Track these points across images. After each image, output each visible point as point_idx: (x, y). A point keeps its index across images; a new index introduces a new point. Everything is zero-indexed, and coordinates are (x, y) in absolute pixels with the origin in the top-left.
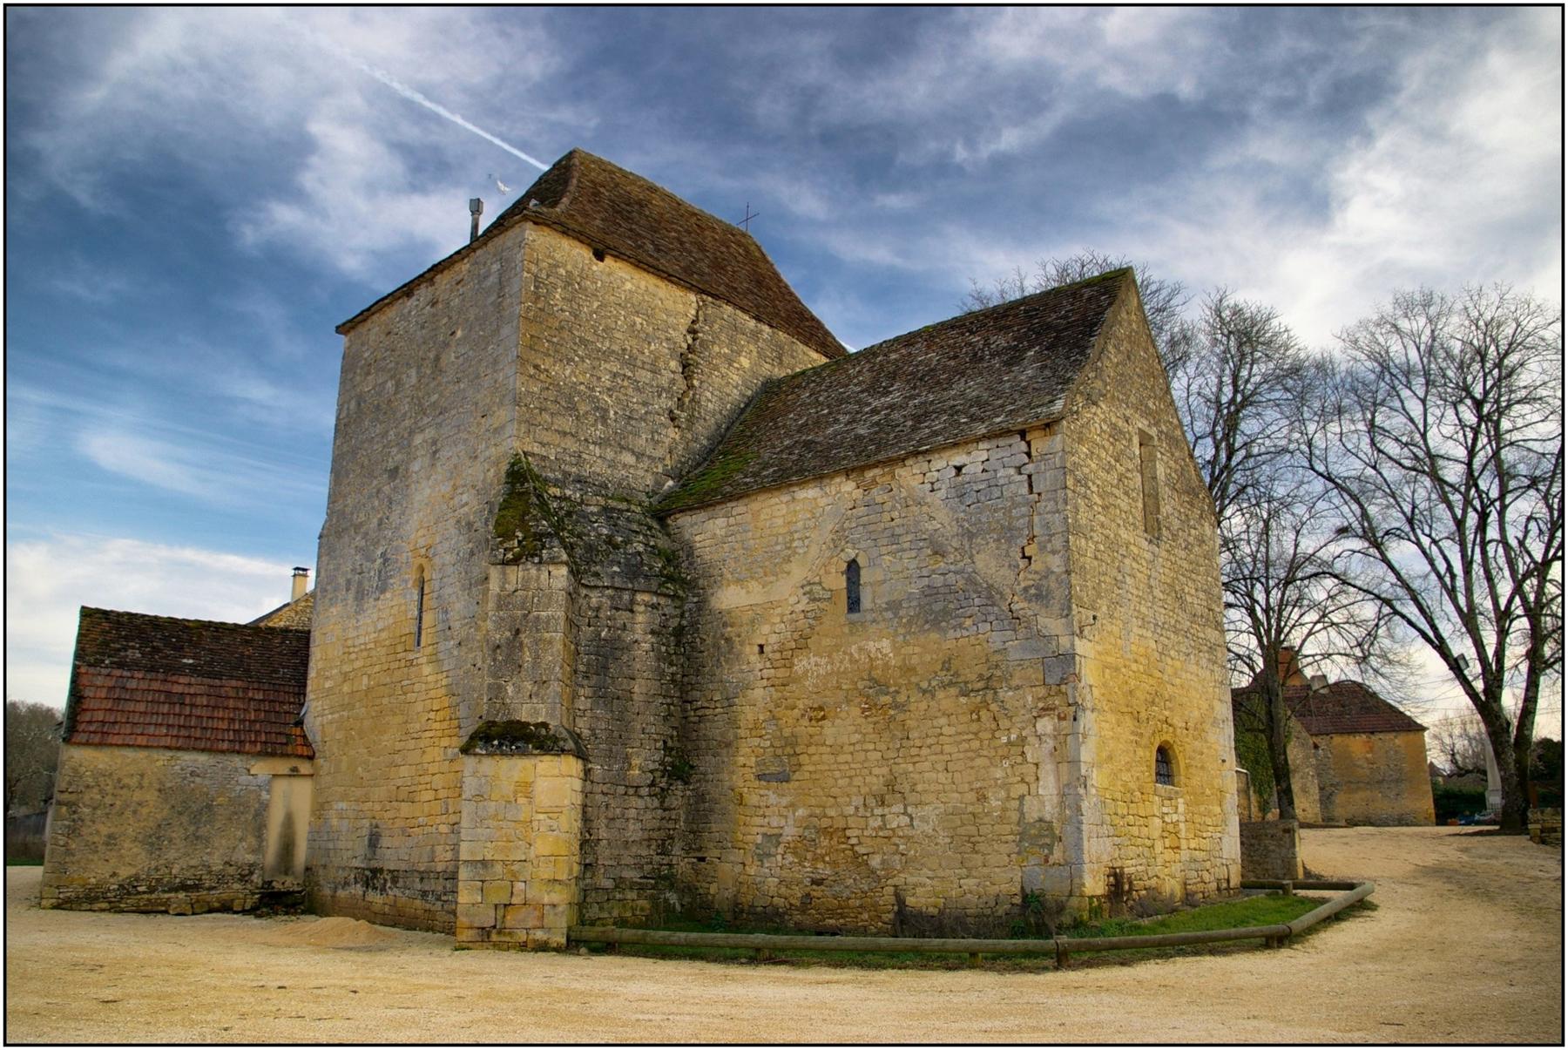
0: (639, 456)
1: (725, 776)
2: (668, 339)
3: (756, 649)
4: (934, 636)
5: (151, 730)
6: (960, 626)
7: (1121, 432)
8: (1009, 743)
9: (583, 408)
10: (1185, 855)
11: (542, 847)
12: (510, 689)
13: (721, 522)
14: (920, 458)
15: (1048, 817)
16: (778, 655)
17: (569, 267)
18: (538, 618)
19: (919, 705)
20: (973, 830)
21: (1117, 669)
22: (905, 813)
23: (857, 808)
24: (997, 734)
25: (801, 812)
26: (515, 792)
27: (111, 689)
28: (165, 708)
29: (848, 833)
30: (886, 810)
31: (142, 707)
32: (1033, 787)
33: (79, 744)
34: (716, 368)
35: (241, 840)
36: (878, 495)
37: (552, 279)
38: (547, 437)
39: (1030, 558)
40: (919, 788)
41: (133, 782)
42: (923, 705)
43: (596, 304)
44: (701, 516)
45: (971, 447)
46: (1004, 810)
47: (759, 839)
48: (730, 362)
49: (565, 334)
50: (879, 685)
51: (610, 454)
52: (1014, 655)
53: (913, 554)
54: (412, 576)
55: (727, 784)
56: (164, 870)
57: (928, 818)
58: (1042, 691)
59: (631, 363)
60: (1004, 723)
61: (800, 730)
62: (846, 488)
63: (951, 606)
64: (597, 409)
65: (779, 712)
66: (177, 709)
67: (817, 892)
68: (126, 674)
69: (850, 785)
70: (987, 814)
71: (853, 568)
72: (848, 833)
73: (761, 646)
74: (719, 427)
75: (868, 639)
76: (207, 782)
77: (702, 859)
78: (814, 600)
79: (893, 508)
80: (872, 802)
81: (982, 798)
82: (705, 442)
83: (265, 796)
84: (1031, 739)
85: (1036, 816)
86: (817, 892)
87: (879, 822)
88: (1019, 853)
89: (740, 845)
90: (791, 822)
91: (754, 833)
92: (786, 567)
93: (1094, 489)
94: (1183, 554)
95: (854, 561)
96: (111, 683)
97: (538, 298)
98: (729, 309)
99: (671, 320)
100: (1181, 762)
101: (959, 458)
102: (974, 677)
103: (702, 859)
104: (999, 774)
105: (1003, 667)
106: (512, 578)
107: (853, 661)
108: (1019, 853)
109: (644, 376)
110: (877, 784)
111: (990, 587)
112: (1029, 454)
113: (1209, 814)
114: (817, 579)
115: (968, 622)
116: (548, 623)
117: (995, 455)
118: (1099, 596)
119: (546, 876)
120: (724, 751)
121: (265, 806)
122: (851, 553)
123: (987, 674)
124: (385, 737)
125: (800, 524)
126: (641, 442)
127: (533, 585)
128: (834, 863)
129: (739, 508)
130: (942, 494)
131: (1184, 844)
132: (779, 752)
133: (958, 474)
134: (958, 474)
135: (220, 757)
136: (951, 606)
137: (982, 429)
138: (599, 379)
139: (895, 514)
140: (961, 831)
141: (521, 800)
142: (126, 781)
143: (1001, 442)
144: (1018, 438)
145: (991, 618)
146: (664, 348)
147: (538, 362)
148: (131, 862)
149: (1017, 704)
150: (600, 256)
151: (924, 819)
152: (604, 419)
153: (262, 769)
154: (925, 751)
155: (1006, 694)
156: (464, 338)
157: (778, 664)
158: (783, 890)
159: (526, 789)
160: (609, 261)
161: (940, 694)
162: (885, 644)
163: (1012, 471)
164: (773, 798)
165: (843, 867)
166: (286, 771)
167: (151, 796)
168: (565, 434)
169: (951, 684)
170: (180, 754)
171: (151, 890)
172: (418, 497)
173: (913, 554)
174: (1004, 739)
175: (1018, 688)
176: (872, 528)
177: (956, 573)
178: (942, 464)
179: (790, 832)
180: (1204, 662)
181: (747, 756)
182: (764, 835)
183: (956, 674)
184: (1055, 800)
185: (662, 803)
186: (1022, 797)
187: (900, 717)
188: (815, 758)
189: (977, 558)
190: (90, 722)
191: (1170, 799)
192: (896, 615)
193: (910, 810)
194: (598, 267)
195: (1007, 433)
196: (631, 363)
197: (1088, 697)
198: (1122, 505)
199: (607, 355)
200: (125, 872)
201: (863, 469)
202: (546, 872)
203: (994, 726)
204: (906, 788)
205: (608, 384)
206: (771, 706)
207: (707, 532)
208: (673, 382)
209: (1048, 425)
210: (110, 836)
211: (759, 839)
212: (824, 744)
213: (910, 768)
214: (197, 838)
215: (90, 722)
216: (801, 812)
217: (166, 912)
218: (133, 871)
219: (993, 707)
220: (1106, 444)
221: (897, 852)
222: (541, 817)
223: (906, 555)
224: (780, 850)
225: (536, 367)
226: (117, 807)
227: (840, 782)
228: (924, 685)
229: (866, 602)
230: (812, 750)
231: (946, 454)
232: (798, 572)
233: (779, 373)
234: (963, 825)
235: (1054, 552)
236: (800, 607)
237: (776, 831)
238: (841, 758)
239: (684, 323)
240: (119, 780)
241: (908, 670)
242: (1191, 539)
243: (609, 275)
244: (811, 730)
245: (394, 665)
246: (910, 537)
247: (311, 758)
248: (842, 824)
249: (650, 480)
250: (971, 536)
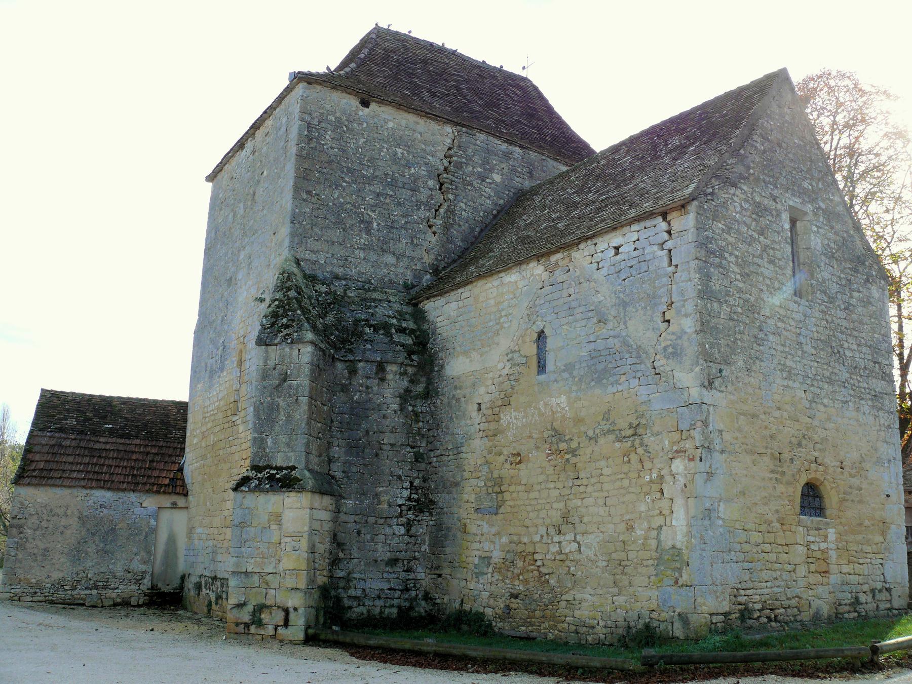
0: (399, 257)
1: (455, 510)
2: (426, 164)
3: (476, 406)
4: (598, 391)
5: (75, 475)
6: (617, 382)
7: (766, 209)
8: (651, 481)
9: (349, 222)
10: (834, 579)
11: (287, 563)
12: (269, 441)
13: (454, 305)
14: (589, 242)
15: (679, 545)
16: (490, 412)
17: (338, 115)
18: (290, 386)
19: (586, 451)
20: (622, 555)
21: (754, 416)
22: (575, 541)
23: (542, 536)
24: (642, 474)
25: (504, 540)
26: (269, 521)
27: (53, 446)
28: (87, 460)
29: (536, 557)
30: (562, 538)
31: (70, 459)
32: (668, 519)
33: (24, 485)
34: (470, 184)
35: (136, 554)
36: (560, 275)
37: (323, 125)
38: (317, 246)
39: (668, 321)
40: (585, 520)
41: (61, 511)
42: (589, 451)
43: (362, 141)
44: (441, 301)
45: (626, 229)
46: (646, 539)
47: (476, 561)
48: (483, 178)
49: (334, 166)
50: (557, 434)
51: (373, 257)
52: (657, 406)
53: (584, 323)
54: (235, 359)
55: (456, 516)
56: (82, 575)
57: (592, 542)
58: (677, 436)
59: (393, 184)
60: (648, 465)
61: (504, 473)
62: (536, 270)
63: (610, 366)
64: (362, 222)
65: (490, 458)
66: (95, 460)
67: (514, 604)
68: (63, 435)
69: (538, 517)
70: (634, 542)
71: (541, 335)
72: (536, 557)
73: (479, 404)
74: (473, 230)
75: (550, 396)
76: (112, 512)
77: (440, 576)
78: (514, 365)
79: (570, 286)
80: (552, 531)
81: (630, 528)
82: (460, 243)
83: (153, 522)
84: (668, 478)
85: (670, 544)
86: (514, 604)
87: (556, 549)
88: (656, 575)
89: (464, 565)
90: (498, 547)
91: (473, 557)
92: (496, 339)
93: (732, 259)
94: (843, 314)
95: (542, 331)
96: (53, 442)
97: (311, 140)
98: (482, 137)
99: (428, 149)
100: (831, 498)
101: (616, 239)
102: (626, 425)
103: (440, 576)
104: (643, 508)
105: (648, 416)
106: (273, 356)
107: (541, 415)
108: (656, 575)
109: (405, 194)
110: (556, 516)
111: (639, 348)
112: (669, 232)
113: (868, 542)
114: (517, 348)
115: (623, 378)
116: (297, 389)
117: (644, 235)
118: (734, 352)
119: (290, 586)
120: (454, 490)
121: (154, 531)
122: (540, 325)
123: (635, 423)
124: (220, 480)
125: (506, 303)
126: (402, 245)
127: (287, 361)
128: (526, 581)
129: (465, 292)
130: (604, 272)
131: (834, 568)
132: (490, 490)
133: (617, 254)
134: (617, 254)
135: (121, 494)
136: (610, 366)
137: (633, 213)
138: (363, 199)
139: (571, 291)
140: (614, 556)
141: (273, 527)
142: (57, 511)
143: (648, 223)
144: (660, 219)
145: (639, 374)
146: (423, 171)
147: (310, 188)
148: (59, 569)
149: (657, 448)
150: (365, 104)
151: (589, 546)
152: (368, 231)
153: (150, 502)
154: (590, 489)
155: (649, 440)
156: (268, 176)
157: (490, 419)
158: (492, 602)
159: (277, 518)
160: (373, 106)
161: (602, 441)
162: (563, 399)
163: (656, 248)
164: (486, 528)
165: (532, 584)
166: (168, 505)
167: (74, 522)
168: (333, 243)
169: (609, 432)
170: (93, 492)
171: (74, 588)
172: (240, 299)
173: (584, 323)
174: (648, 478)
175: (658, 434)
176: (555, 303)
177: (614, 337)
178: (605, 243)
179: (497, 556)
180: (866, 409)
181: (471, 491)
182: (480, 557)
183: (613, 424)
184: (685, 529)
185: (408, 531)
186: (661, 527)
187: (573, 460)
188: (514, 495)
189: (630, 323)
190: (34, 470)
191: (818, 529)
192: (571, 374)
193: (578, 537)
194: (364, 112)
195: (650, 215)
196: (393, 184)
197: (718, 441)
198: (766, 272)
199: (370, 180)
200: (56, 575)
201: (549, 253)
202: (290, 582)
203: (640, 467)
204: (576, 519)
205: (372, 202)
206: (485, 453)
207: (443, 312)
208: (431, 197)
209: (683, 206)
210: (46, 550)
211: (476, 561)
212: (520, 484)
213: (579, 502)
214: (106, 552)
215: (34, 470)
216: (504, 540)
217: (83, 605)
218: (61, 575)
219: (640, 451)
220: (748, 220)
221: (568, 573)
222: (289, 539)
223: (579, 324)
224: (490, 570)
225: (309, 192)
226: (50, 530)
227: (531, 514)
228: (590, 433)
229: (550, 366)
230: (512, 488)
231: (607, 237)
232: (505, 343)
233: (527, 184)
234: (616, 551)
235: (686, 316)
236: (506, 371)
237: (488, 554)
238: (532, 495)
239: (441, 151)
240: (51, 511)
241: (579, 421)
242: (853, 301)
243: (373, 118)
244: (512, 472)
245: (226, 426)
246: (582, 309)
247: (186, 495)
248: (531, 550)
249: (409, 276)
250: (625, 304)
